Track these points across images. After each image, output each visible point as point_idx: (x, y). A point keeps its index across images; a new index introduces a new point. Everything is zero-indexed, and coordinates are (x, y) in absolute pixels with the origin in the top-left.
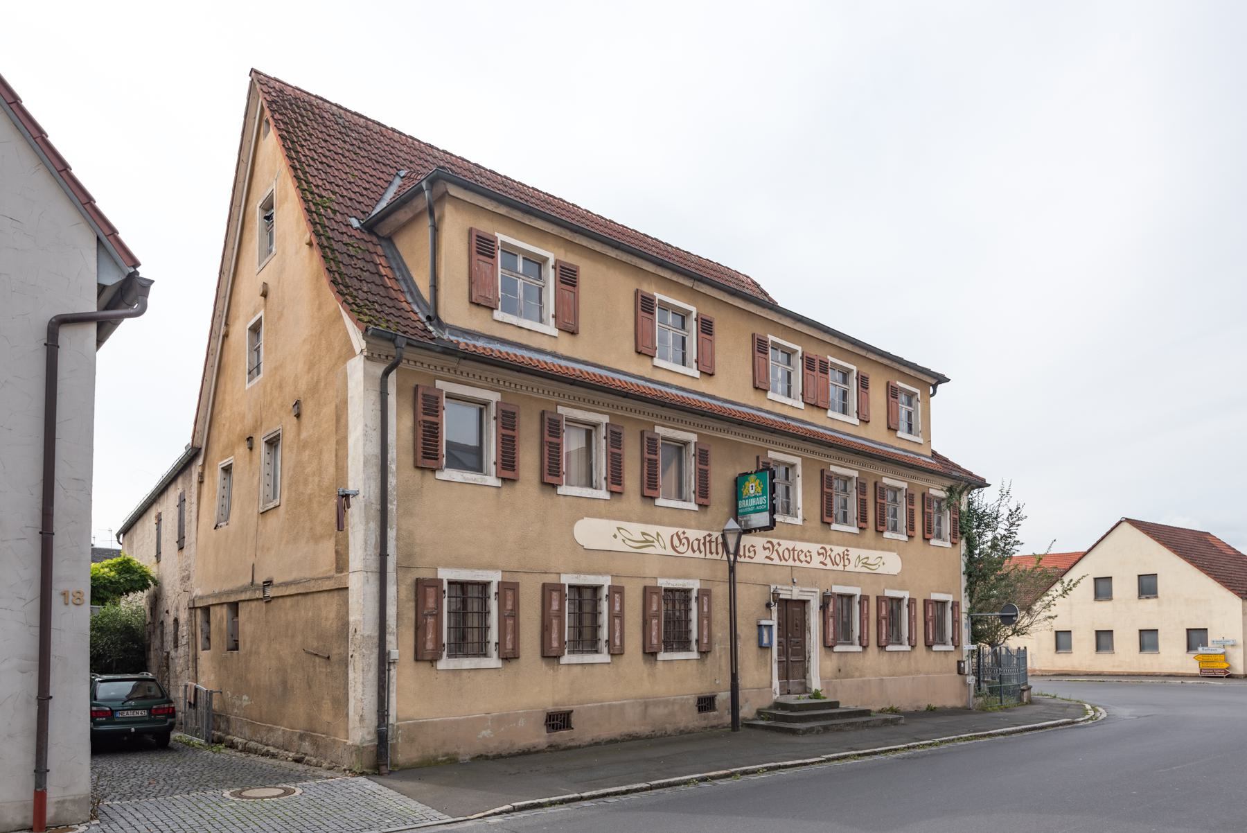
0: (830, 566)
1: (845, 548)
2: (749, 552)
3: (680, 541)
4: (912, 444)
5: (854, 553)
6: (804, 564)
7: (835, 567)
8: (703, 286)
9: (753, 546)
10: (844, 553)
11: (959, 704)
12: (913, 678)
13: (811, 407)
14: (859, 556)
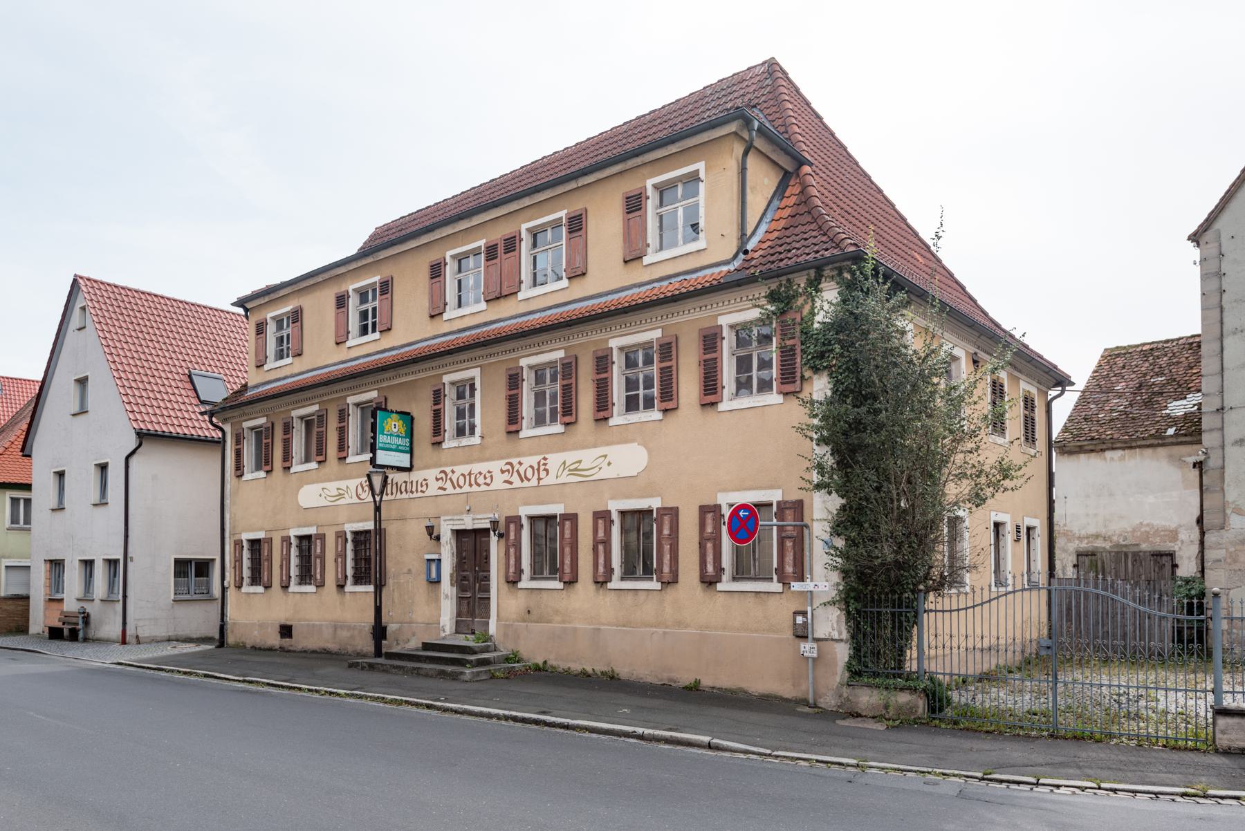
0: (450, 490)
1: (540, 457)
2: (422, 486)
3: (363, 488)
4: (555, 295)
5: (554, 460)
6: (484, 488)
7: (526, 484)
8: (380, 253)
9: (425, 480)
10: (539, 463)
11: (787, 691)
12: (665, 633)
13: (498, 301)
14: (564, 463)
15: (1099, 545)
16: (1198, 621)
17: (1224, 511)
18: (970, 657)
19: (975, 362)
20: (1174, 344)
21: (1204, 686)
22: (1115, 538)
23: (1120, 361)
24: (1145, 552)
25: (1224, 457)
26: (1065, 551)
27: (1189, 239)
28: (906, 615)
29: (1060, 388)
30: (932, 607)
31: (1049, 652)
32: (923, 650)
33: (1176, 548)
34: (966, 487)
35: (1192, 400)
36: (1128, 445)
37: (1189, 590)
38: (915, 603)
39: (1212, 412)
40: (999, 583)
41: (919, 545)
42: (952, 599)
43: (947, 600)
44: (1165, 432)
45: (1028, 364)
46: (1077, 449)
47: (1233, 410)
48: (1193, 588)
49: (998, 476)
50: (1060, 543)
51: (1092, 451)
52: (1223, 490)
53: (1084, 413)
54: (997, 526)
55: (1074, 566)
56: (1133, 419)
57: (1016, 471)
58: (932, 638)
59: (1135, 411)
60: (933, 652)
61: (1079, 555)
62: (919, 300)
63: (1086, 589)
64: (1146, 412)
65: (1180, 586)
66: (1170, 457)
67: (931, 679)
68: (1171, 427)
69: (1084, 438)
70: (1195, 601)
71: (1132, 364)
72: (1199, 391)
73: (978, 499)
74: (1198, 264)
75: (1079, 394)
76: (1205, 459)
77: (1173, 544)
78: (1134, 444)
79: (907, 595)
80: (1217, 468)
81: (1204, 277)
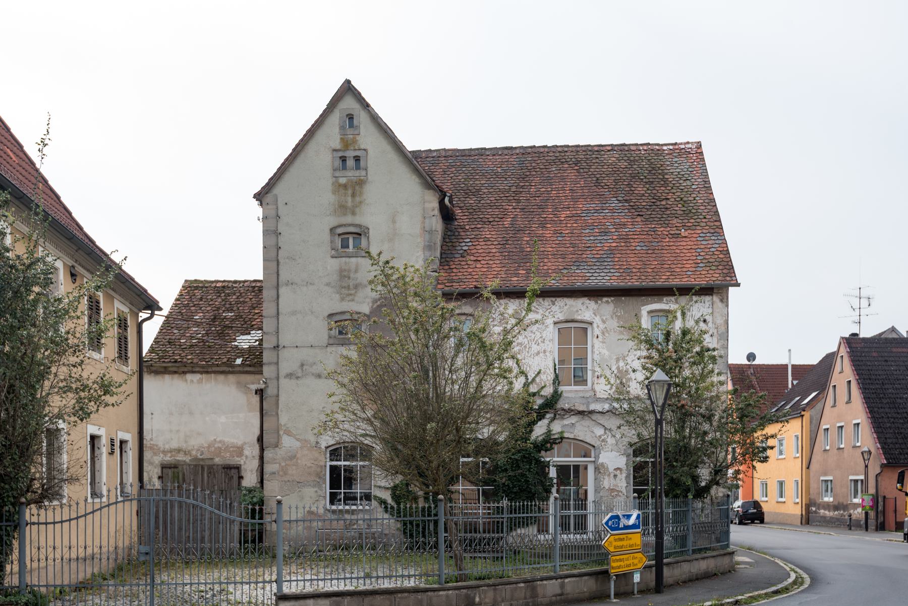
15: (180, 459)
16: (259, 524)
17: (278, 432)
18: (66, 568)
19: (73, 275)
20: (241, 285)
21: (251, 572)
22: (194, 453)
23: (198, 293)
24: (218, 465)
25: (278, 387)
26: (151, 463)
27: (254, 197)
28: (6, 529)
29: (150, 312)
30: (34, 519)
31: (148, 558)
32: (25, 563)
33: (242, 462)
34: (70, 400)
35: (256, 335)
36: (205, 370)
37: (252, 498)
38: (16, 516)
39: (270, 348)
40: (94, 494)
41: (20, 457)
42: (56, 512)
43: (50, 513)
44: (235, 362)
45: (122, 285)
46: (163, 370)
47: (286, 349)
48: (255, 496)
49: (99, 391)
50: (147, 455)
51: (175, 372)
52: (277, 414)
53: (168, 337)
54: (93, 438)
55: (159, 478)
56: (209, 347)
57: (116, 387)
58: (34, 551)
59: (211, 340)
60: (35, 565)
61: (164, 467)
62: (17, 202)
63: (181, 499)
64: (219, 342)
65: (245, 495)
66: (239, 383)
67: (33, 592)
68: (239, 357)
69: (168, 360)
70: (257, 508)
71: (208, 297)
72: (261, 329)
73: (82, 414)
74: (261, 220)
75: (164, 318)
76: (265, 388)
77: (239, 459)
78: (210, 370)
79: (7, 508)
80: (273, 396)
81: (266, 233)
